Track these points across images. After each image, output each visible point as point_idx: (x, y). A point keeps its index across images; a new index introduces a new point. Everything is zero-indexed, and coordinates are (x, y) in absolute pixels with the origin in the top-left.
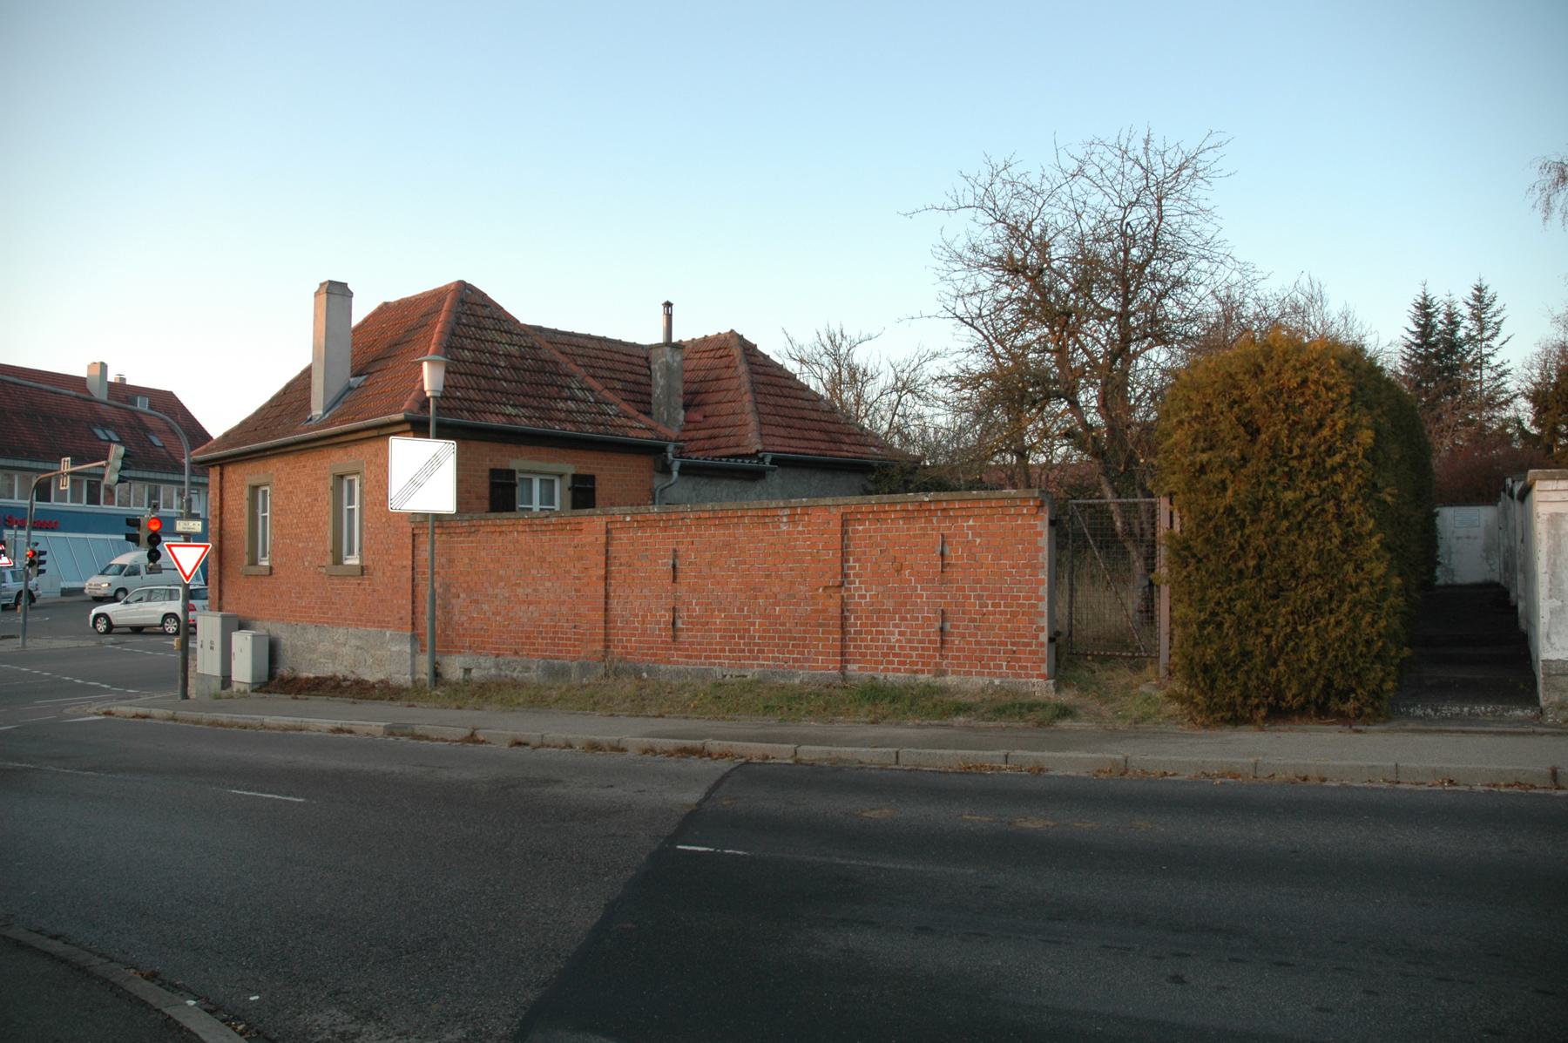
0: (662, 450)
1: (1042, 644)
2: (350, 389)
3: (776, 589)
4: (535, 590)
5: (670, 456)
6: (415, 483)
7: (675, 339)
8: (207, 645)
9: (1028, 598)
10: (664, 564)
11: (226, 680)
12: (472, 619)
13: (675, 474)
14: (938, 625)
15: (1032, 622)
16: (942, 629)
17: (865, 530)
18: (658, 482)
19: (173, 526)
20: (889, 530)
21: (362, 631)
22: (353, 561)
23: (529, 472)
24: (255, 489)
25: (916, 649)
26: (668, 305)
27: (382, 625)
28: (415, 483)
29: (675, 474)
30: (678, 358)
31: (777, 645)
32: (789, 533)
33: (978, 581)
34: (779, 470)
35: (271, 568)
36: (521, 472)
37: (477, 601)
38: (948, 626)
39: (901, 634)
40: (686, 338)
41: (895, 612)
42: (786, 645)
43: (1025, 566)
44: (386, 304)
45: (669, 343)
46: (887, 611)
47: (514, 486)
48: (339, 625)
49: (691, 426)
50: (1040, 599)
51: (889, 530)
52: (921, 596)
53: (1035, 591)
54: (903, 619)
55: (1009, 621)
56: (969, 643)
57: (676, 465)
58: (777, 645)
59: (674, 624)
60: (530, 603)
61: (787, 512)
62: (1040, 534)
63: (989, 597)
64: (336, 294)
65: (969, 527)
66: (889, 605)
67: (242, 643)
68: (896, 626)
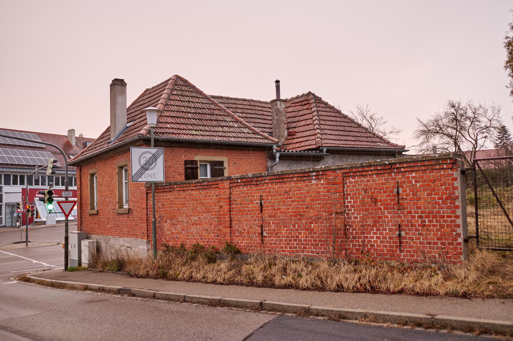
0: (270, 148)
1: (459, 244)
2: (127, 127)
3: (312, 214)
4: (200, 218)
5: (274, 151)
6: (144, 168)
7: (282, 97)
8: (73, 246)
9: (450, 217)
10: (257, 203)
11: (80, 264)
12: (172, 233)
13: (278, 159)
14: (397, 233)
15: (453, 230)
16: (400, 235)
17: (356, 182)
18: (269, 164)
19: (61, 194)
20: (368, 181)
21: (130, 239)
22: (126, 207)
23: (204, 161)
24: (92, 175)
25: (386, 246)
26: (277, 82)
27: (136, 236)
28: (144, 168)
29: (278, 159)
30: (283, 106)
31: (312, 245)
32: (316, 185)
33: (419, 208)
34: (331, 156)
35: (129, 209)
36: (200, 161)
37: (174, 224)
38: (403, 233)
39: (377, 237)
40: (289, 97)
41: (373, 226)
42: (317, 245)
43: (447, 198)
44: (148, 90)
45: (278, 99)
46: (369, 225)
47: (197, 168)
48: (121, 236)
49: (291, 137)
50: (457, 217)
51: (368, 181)
52: (387, 217)
53: (454, 212)
54: (378, 230)
55: (438, 230)
56: (415, 243)
57: (278, 155)
58: (312, 245)
59: (262, 233)
60: (197, 225)
61: (314, 174)
62: (455, 179)
63: (427, 217)
64: (118, 85)
65: (413, 177)
66: (370, 222)
67: (85, 243)
68: (374, 233)
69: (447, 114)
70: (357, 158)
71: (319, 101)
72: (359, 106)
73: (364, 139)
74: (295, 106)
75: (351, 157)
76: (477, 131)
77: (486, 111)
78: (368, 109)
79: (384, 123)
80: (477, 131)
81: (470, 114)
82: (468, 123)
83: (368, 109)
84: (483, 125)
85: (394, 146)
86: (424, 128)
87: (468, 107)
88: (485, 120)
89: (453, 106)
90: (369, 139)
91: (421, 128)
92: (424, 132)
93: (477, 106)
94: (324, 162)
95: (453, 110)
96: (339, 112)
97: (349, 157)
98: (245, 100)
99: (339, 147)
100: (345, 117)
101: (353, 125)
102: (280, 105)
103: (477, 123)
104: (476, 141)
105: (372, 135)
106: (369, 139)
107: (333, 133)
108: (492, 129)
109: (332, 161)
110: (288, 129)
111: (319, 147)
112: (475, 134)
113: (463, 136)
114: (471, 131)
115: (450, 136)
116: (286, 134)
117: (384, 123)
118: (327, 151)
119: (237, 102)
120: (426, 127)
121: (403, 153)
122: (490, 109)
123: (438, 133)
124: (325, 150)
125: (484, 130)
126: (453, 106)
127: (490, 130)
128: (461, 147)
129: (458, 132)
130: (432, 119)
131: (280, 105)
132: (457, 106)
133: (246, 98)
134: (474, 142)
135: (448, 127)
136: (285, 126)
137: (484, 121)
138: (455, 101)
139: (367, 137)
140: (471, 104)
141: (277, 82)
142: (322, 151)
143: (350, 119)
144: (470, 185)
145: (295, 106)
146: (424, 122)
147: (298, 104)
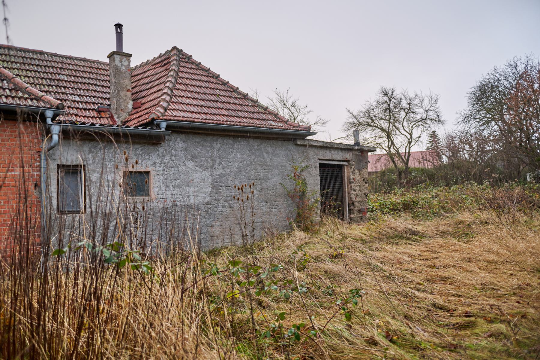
13: (55, 138)
26: (119, 26)
29: (55, 138)
69: (379, 103)
70: (231, 142)
71: (186, 60)
72: (277, 90)
73: (246, 115)
74: (155, 68)
75: (220, 140)
76: (412, 124)
77: (422, 101)
78: (289, 95)
79: (309, 112)
80: (412, 124)
81: (404, 104)
82: (403, 114)
83: (289, 95)
84: (418, 117)
85: (294, 127)
86: (355, 121)
87: (403, 97)
88: (422, 110)
89: (386, 94)
90: (256, 116)
91: (351, 120)
92: (354, 125)
93: (412, 95)
94: (167, 147)
95: (386, 98)
96: (217, 77)
97: (217, 141)
98: (85, 60)
99: (194, 121)
100: (226, 83)
101: (234, 95)
102: (121, 61)
103: (412, 115)
104: (411, 134)
105: (261, 110)
106: (256, 116)
107: (194, 102)
108: (428, 121)
109: (184, 145)
110: (134, 100)
111: (153, 119)
112: (410, 127)
113: (397, 129)
114: (405, 124)
115: (382, 129)
116: (130, 106)
117: (309, 112)
118: (167, 128)
119: (65, 60)
120: (356, 118)
121: (308, 138)
122: (426, 98)
123: (369, 125)
124: (164, 125)
125: (420, 123)
126: (386, 94)
127: (425, 123)
128: (394, 142)
129: (391, 125)
130: (364, 110)
131: (121, 61)
132: (390, 93)
133: (87, 58)
134: (409, 137)
135: (381, 119)
136: (129, 94)
137: (420, 113)
138: (389, 88)
139: (253, 113)
140: (405, 94)
141: (119, 26)
142: (158, 126)
143: (232, 87)
144: (405, 184)
145: (155, 68)
146: (355, 113)
147: (157, 66)
